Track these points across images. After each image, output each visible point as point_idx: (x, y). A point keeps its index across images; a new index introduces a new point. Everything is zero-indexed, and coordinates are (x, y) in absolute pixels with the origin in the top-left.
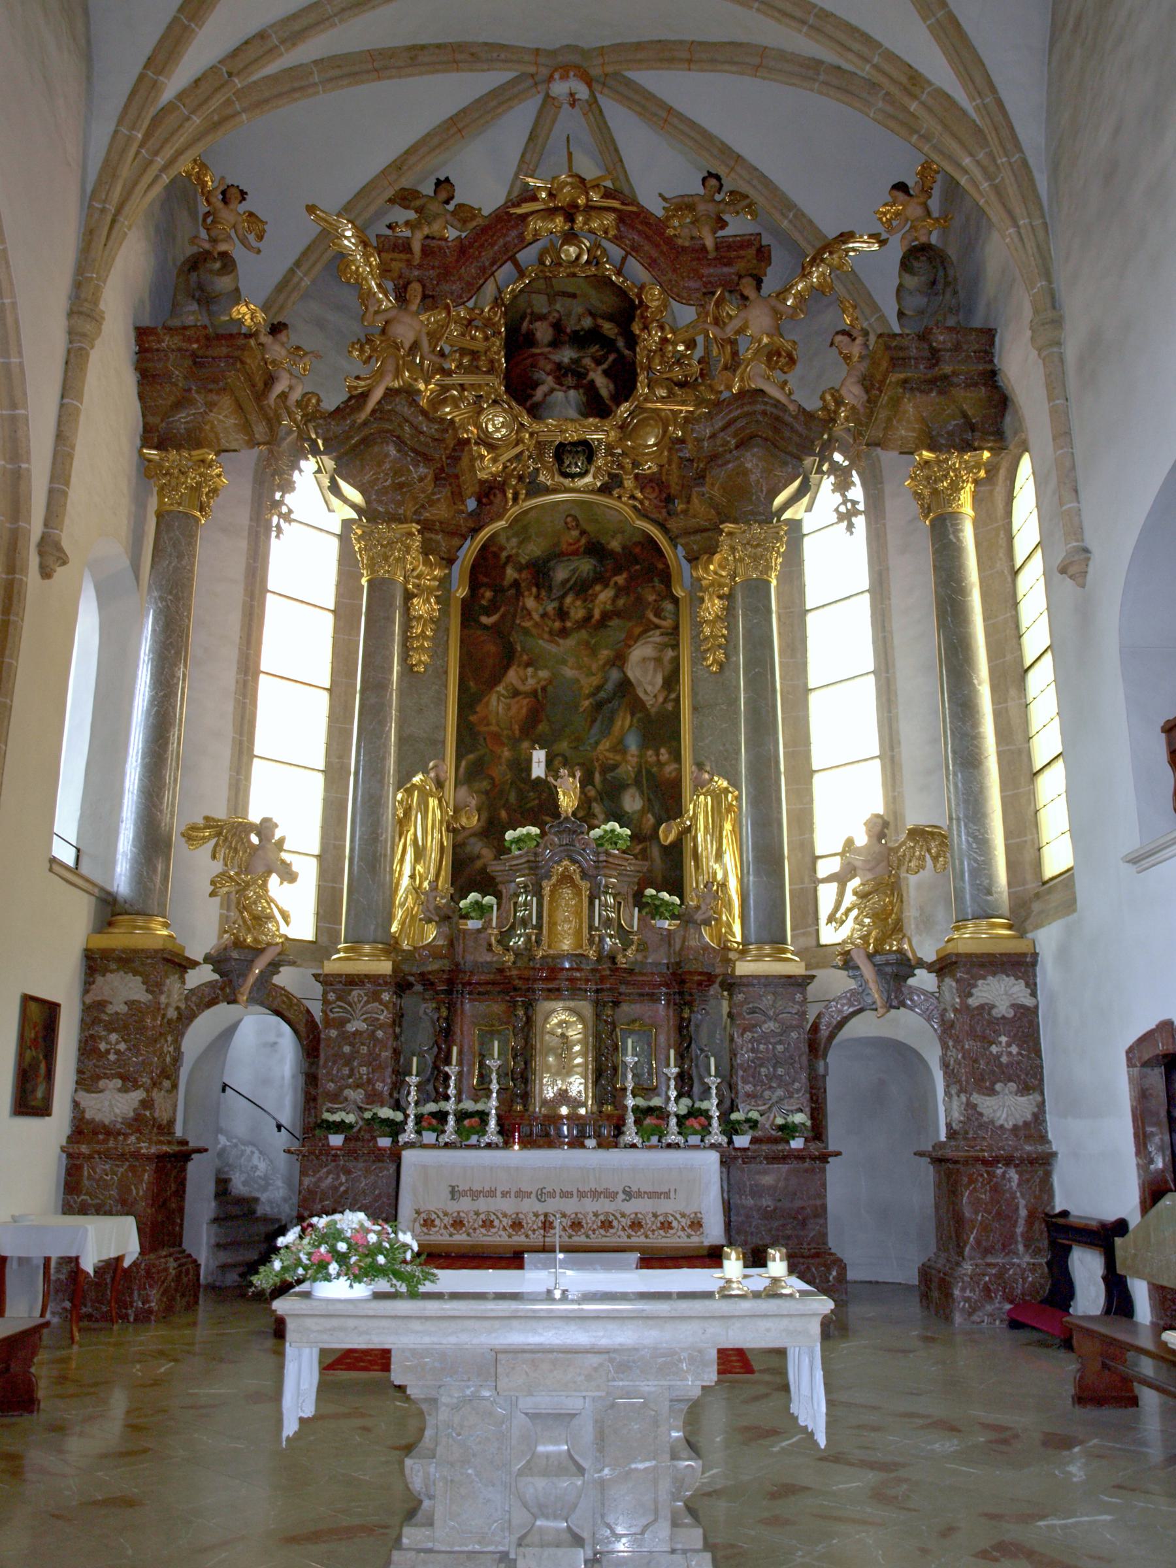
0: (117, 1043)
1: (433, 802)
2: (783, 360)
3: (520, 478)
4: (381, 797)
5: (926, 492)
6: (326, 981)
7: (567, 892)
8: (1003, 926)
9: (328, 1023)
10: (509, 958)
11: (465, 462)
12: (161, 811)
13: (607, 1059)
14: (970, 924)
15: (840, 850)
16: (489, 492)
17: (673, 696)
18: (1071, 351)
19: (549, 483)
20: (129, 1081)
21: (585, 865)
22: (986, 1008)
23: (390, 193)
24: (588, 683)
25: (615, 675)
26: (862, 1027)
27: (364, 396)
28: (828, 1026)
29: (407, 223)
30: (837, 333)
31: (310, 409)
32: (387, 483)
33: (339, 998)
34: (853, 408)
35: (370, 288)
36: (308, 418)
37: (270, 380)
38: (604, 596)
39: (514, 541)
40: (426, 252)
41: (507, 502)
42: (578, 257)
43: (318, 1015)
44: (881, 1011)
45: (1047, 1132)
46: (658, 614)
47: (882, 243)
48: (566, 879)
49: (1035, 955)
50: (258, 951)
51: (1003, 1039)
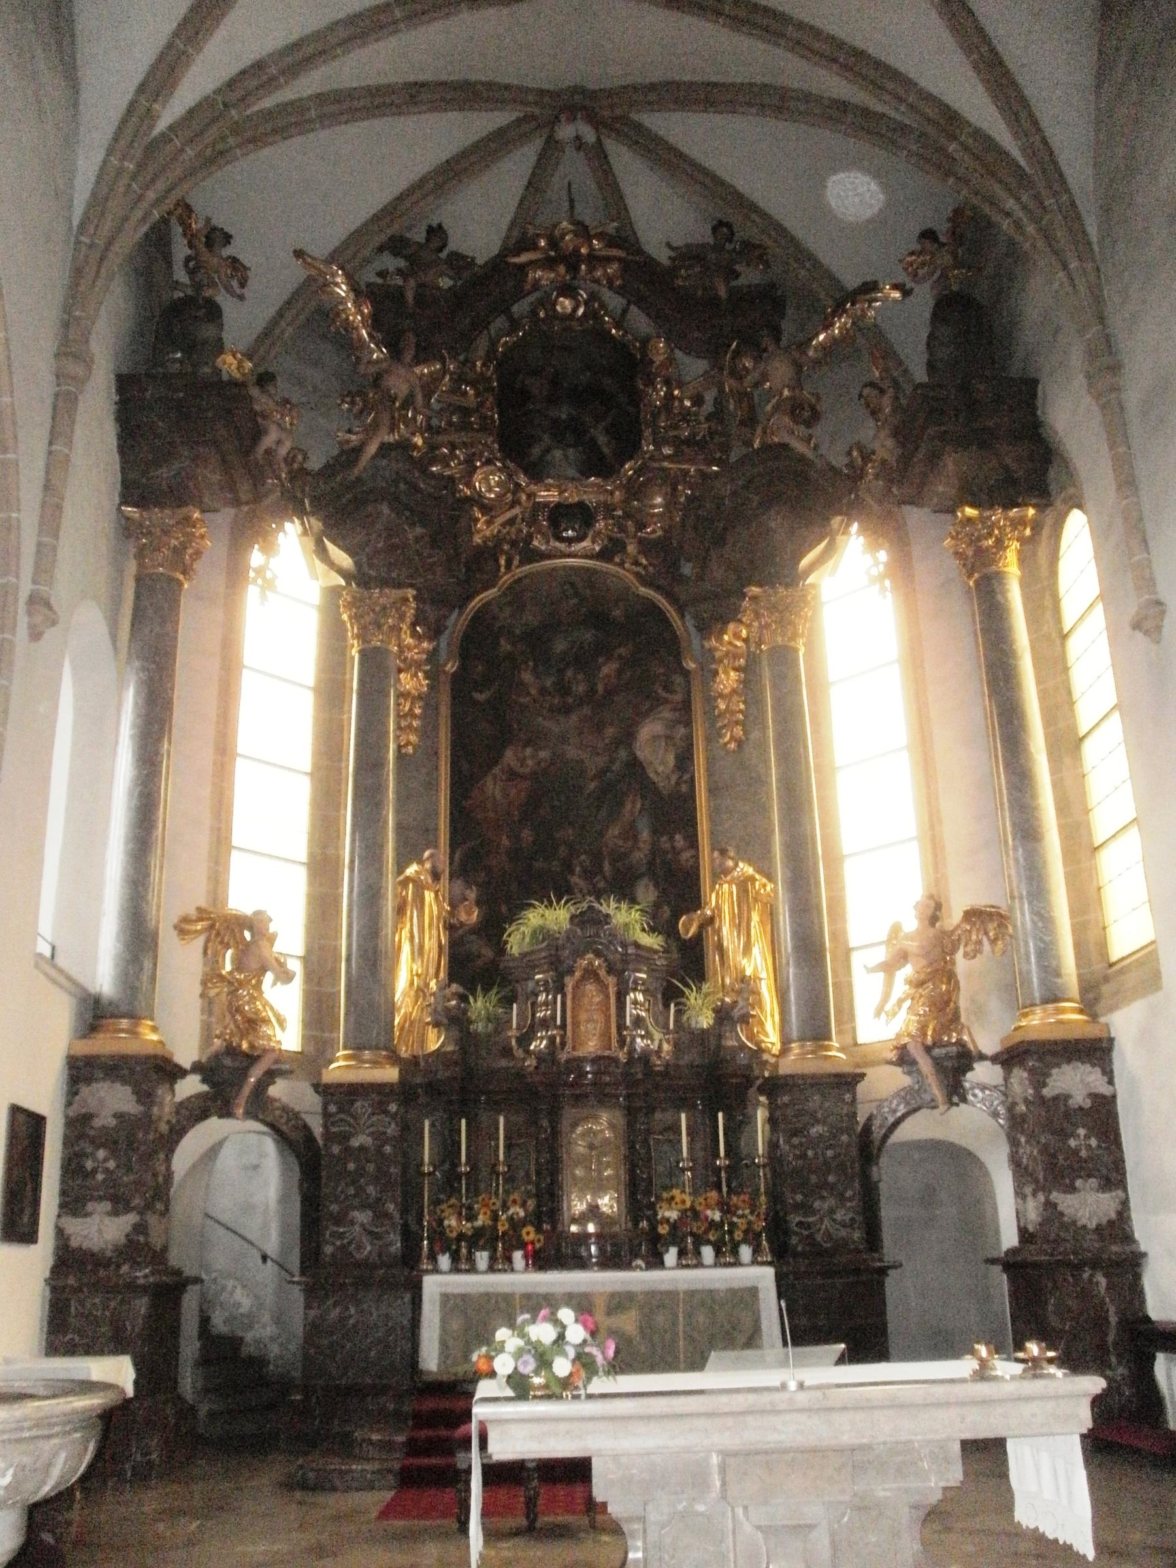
0: (106, 1160)
1: (429, 896)
2: (806, 414)
3: (513, 544)
4: (380, 888)
5: (970, 553)
6: (326, 1091)
7: (590, 988)
8: (1073, 1010)
9: (327, 1135)
10: (530, 1063)
11: (463, 523)
12: (147, 903)
13: (642, 1172)
14: (1038, 1010)
15: (885, 938)
16: (486, 555)
17: (686, 777)
18: (1132, 397)
19: (543, 548)
20: (120, 1205)
21: (611, 957)
22: (1064, 1098)
23: (382, 238)
24: (593, 764)
25: (623, 754)
26: (915, 1129)
27: (358, 450)
28: (881, 1126)
29: (399, 271)
30: (866, 386)
31: (296, 466)
32: (380, 545)
33: (341, 1110)
34: (884, 462)
35: (360, 337)
36: (293, 476)
37: (257, 434)
38: (608, 669)
39: (507, 611)
40: (420, 300)
41: (499, 570)
42: (575, 310)
43: (318, 1130)
44: (942, 1108)
45: (1132, 1231)
46: (666, 688)
47: (906, 293)
48: (591, 974)
49: (1111, 1040)
50: (251, 1059)
51: (1082, 1132)
